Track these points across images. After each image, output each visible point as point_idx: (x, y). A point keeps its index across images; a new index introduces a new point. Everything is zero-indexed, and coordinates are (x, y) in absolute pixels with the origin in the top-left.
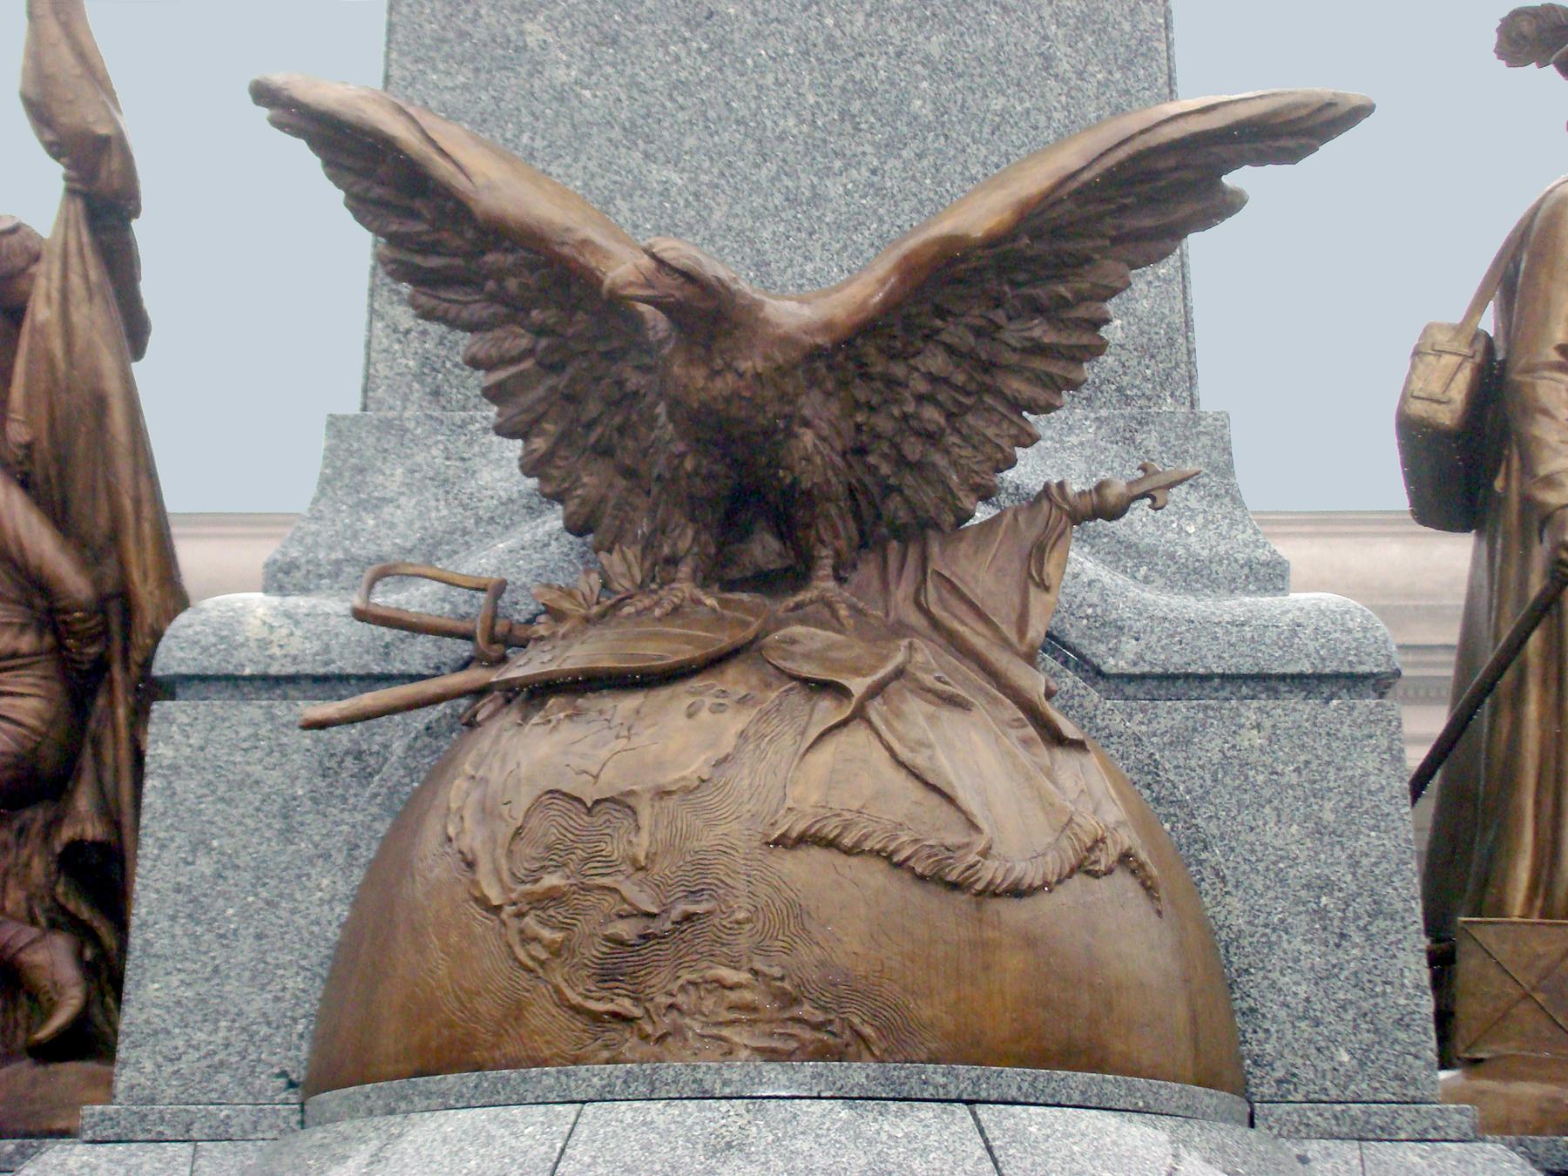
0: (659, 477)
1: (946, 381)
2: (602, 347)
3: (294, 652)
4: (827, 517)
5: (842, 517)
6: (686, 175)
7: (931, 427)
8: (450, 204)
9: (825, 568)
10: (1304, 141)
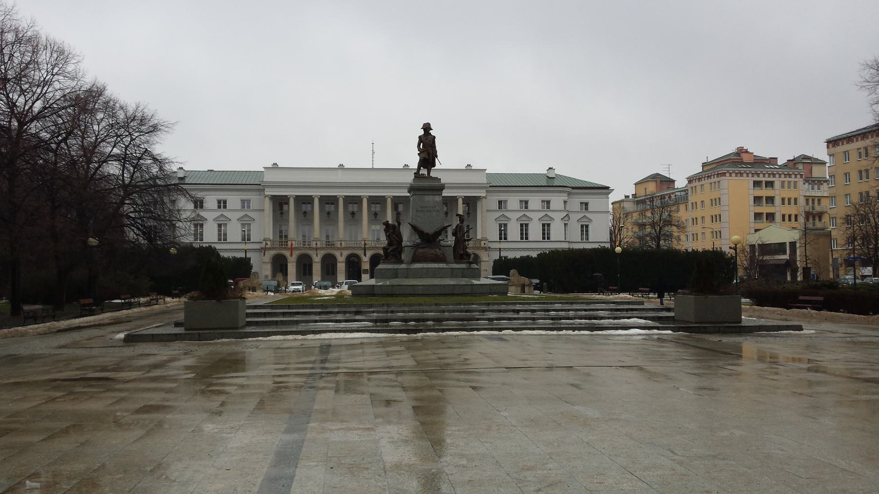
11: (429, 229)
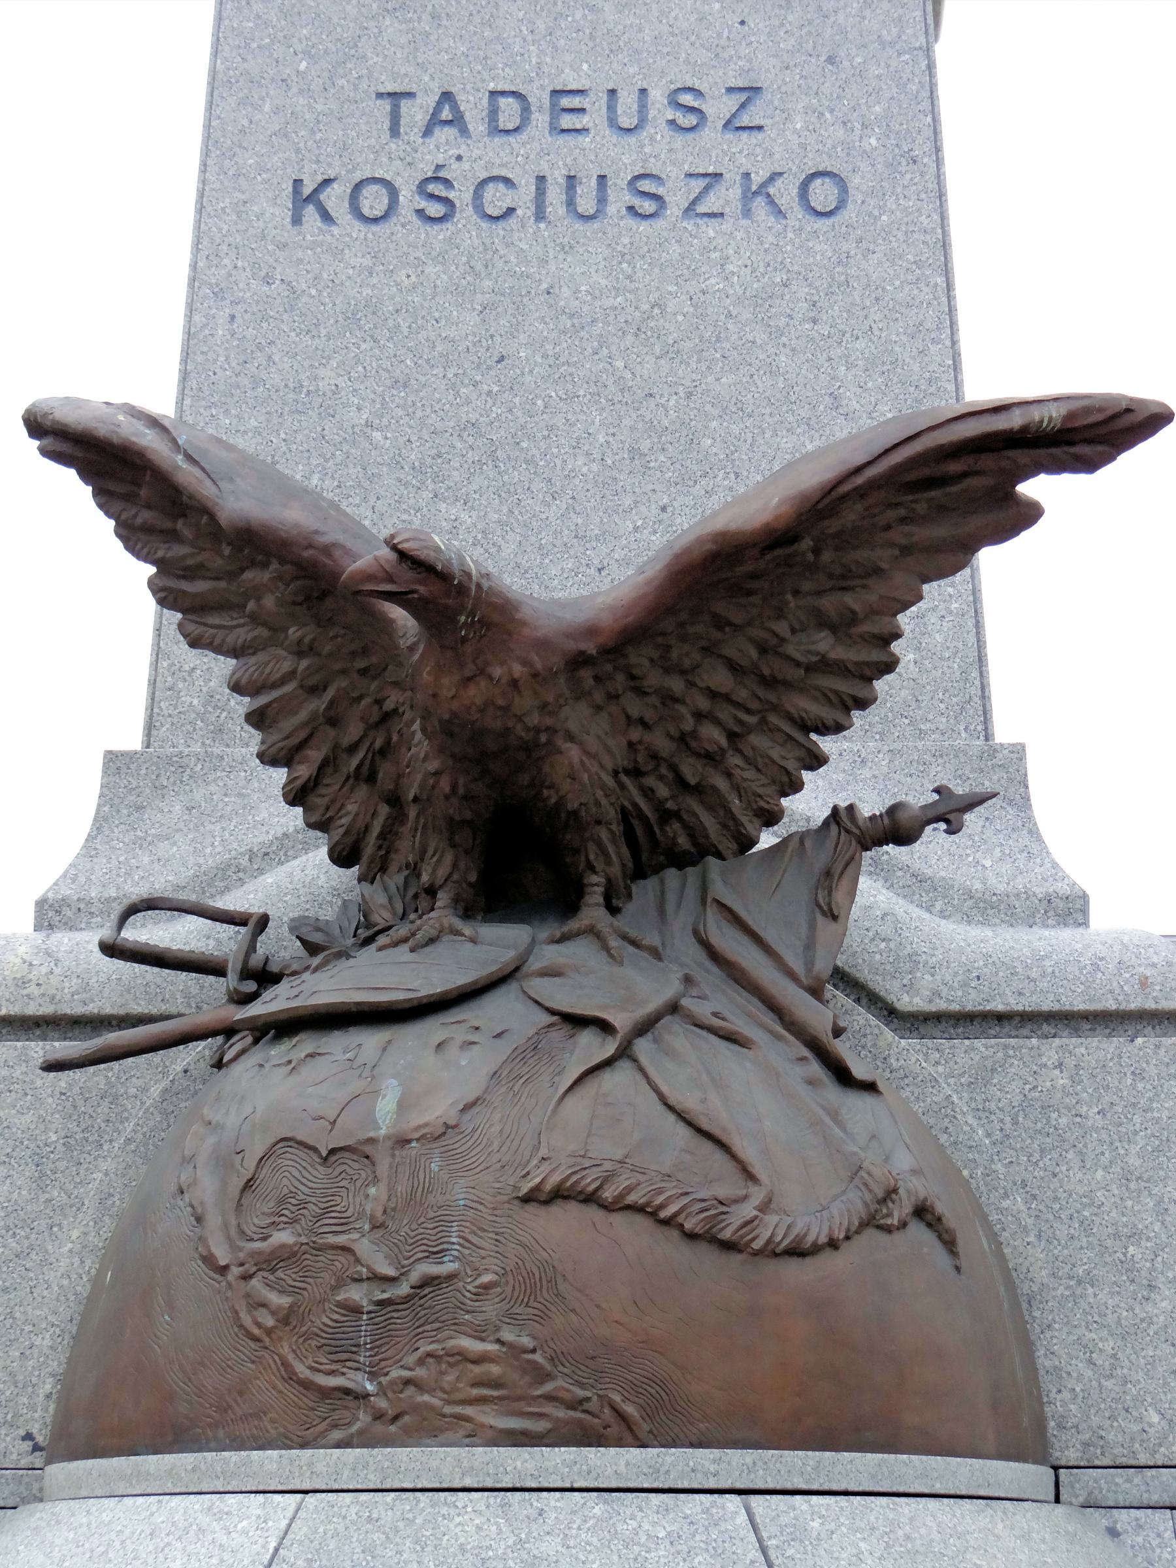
0: (416, 799)
1: (727, 698)
2: (360, 664)
3: (52, 992)
4: (599, 843)
5: (614, 841)
6: (474, 514)
7: (712, 748)
8: (205, 519)
9: (595, 896)
10: (1100, 448)
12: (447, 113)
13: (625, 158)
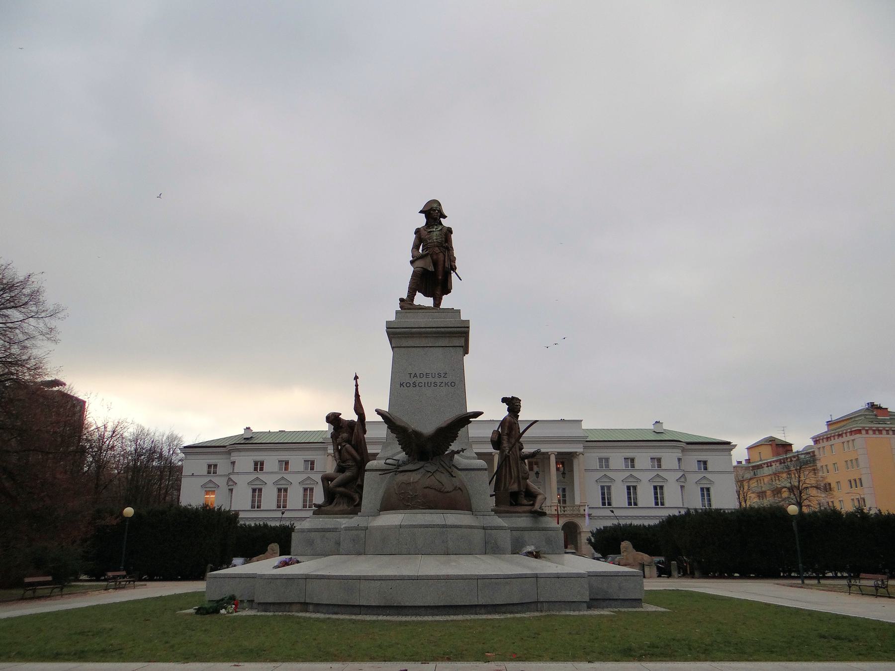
11: (427, 425)
12: (415, 375)
13: (433, 380)
